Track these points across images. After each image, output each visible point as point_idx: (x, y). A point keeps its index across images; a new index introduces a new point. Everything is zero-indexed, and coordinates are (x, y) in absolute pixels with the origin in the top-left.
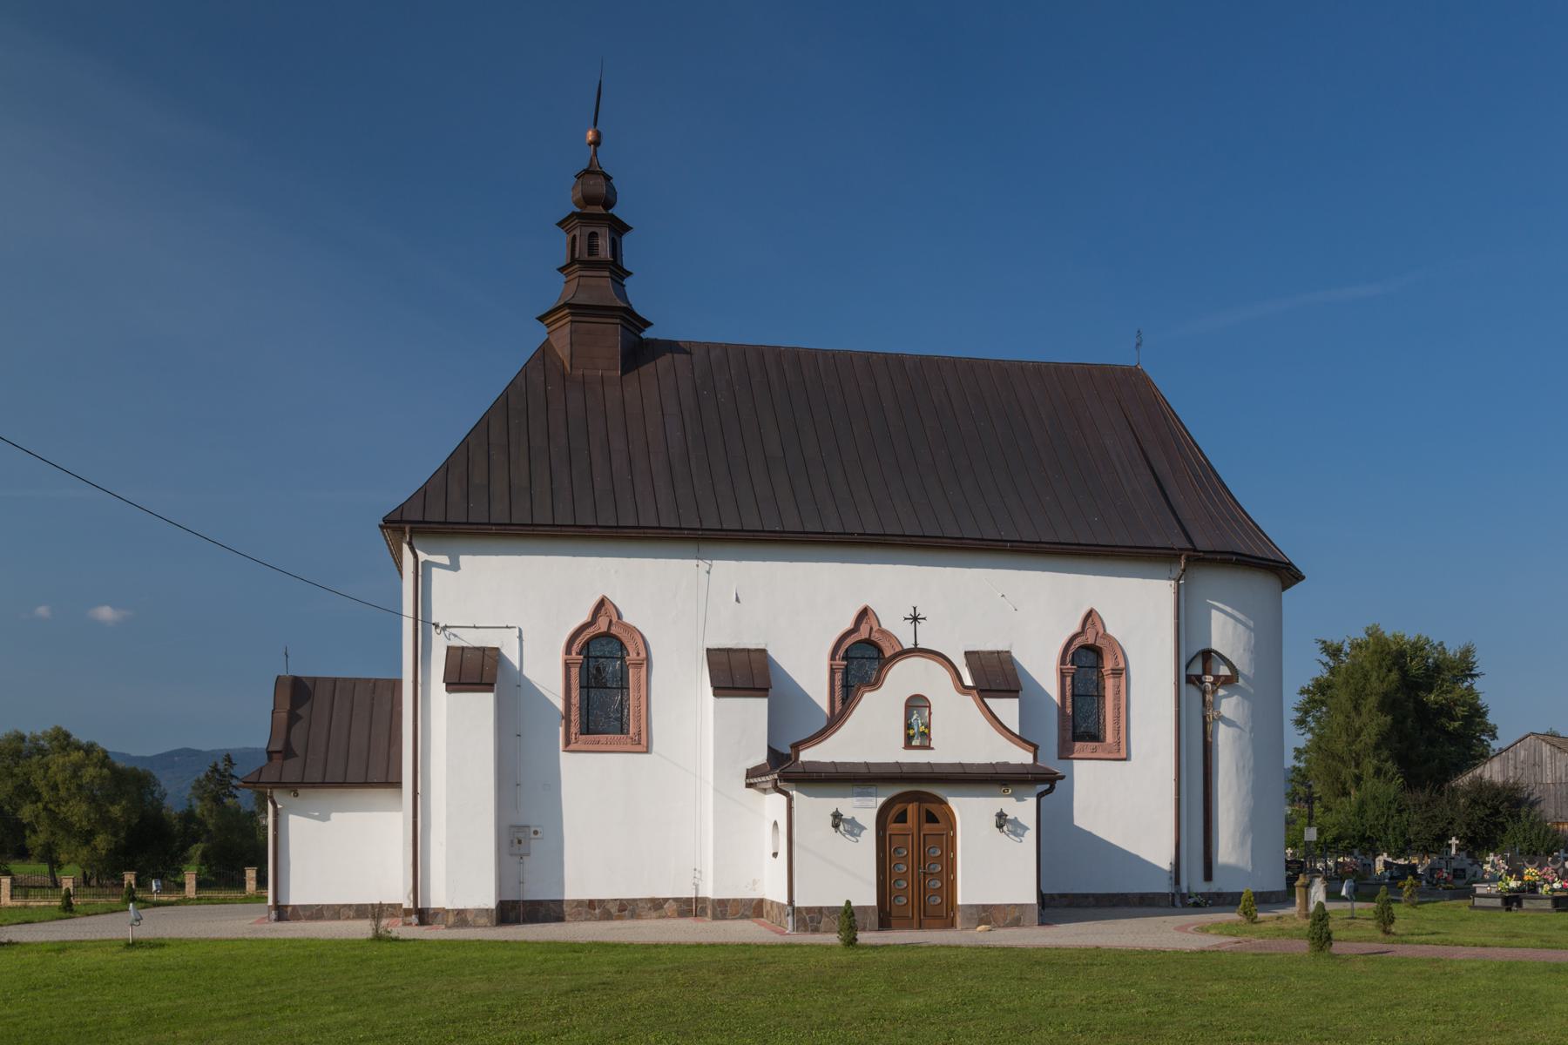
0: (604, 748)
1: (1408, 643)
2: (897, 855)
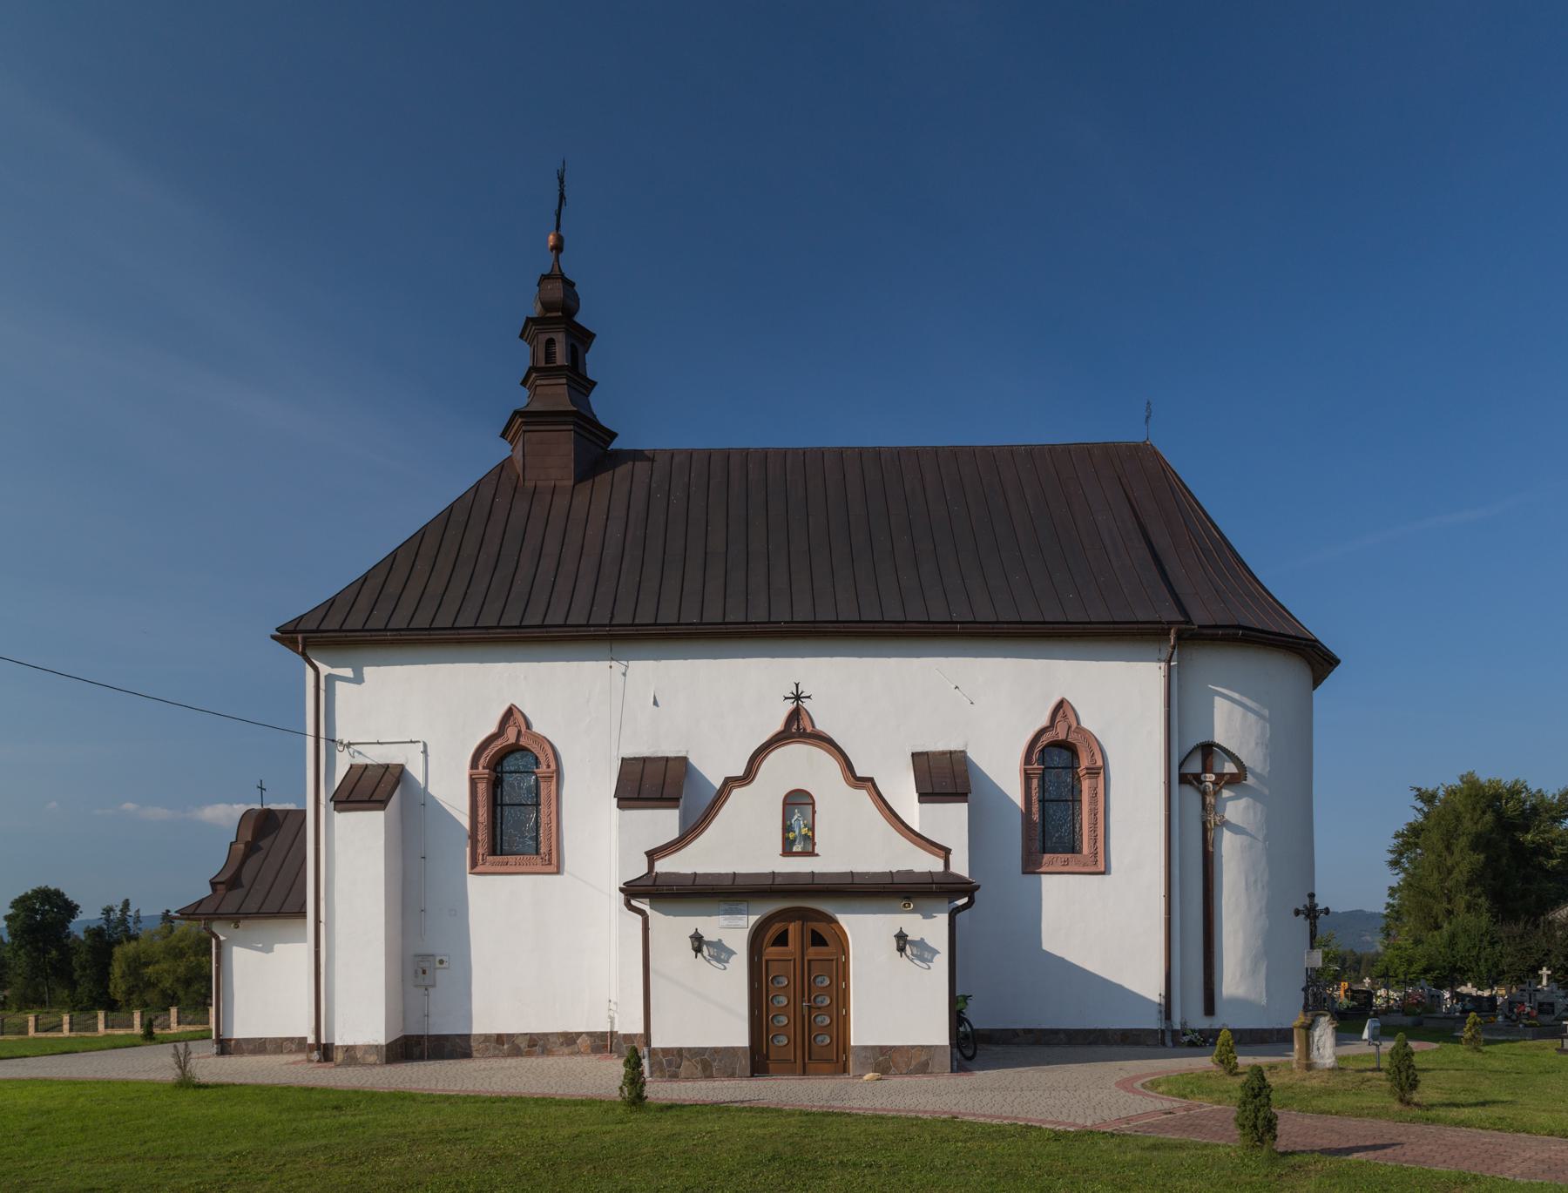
0: (512, 869)
1: (1504, 787)
2: (776, 985)
